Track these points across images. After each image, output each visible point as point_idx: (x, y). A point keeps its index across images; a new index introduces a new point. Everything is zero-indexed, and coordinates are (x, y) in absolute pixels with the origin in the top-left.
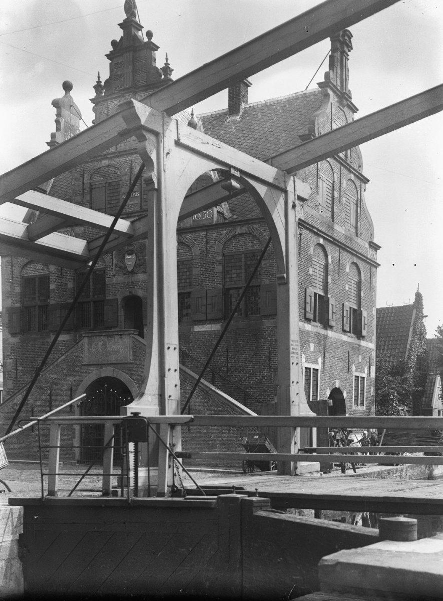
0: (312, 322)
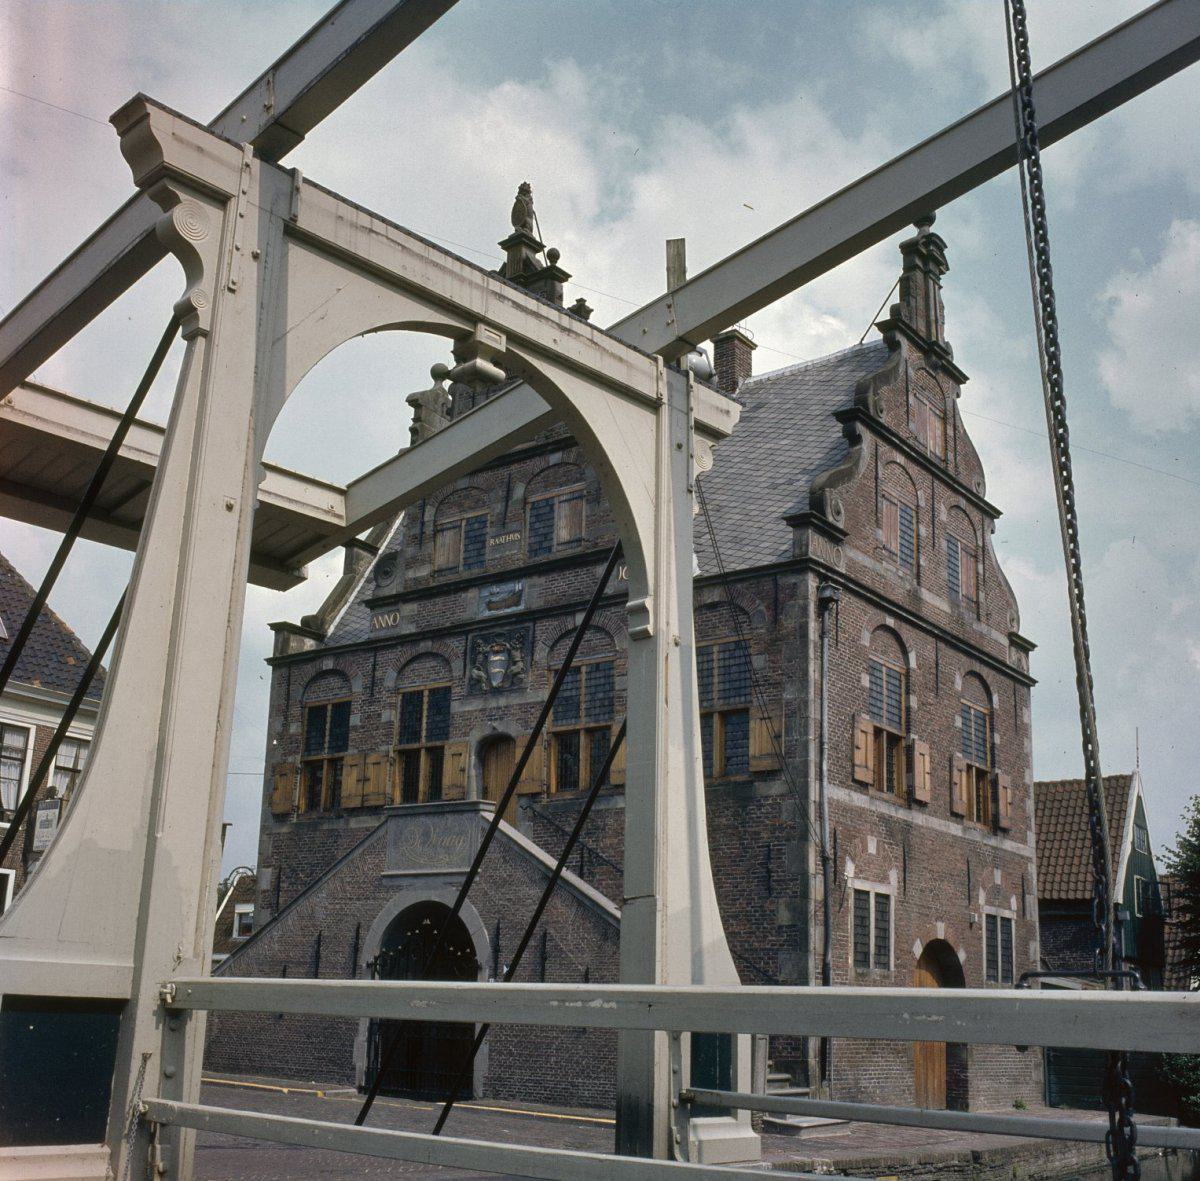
0: (872, 791)
